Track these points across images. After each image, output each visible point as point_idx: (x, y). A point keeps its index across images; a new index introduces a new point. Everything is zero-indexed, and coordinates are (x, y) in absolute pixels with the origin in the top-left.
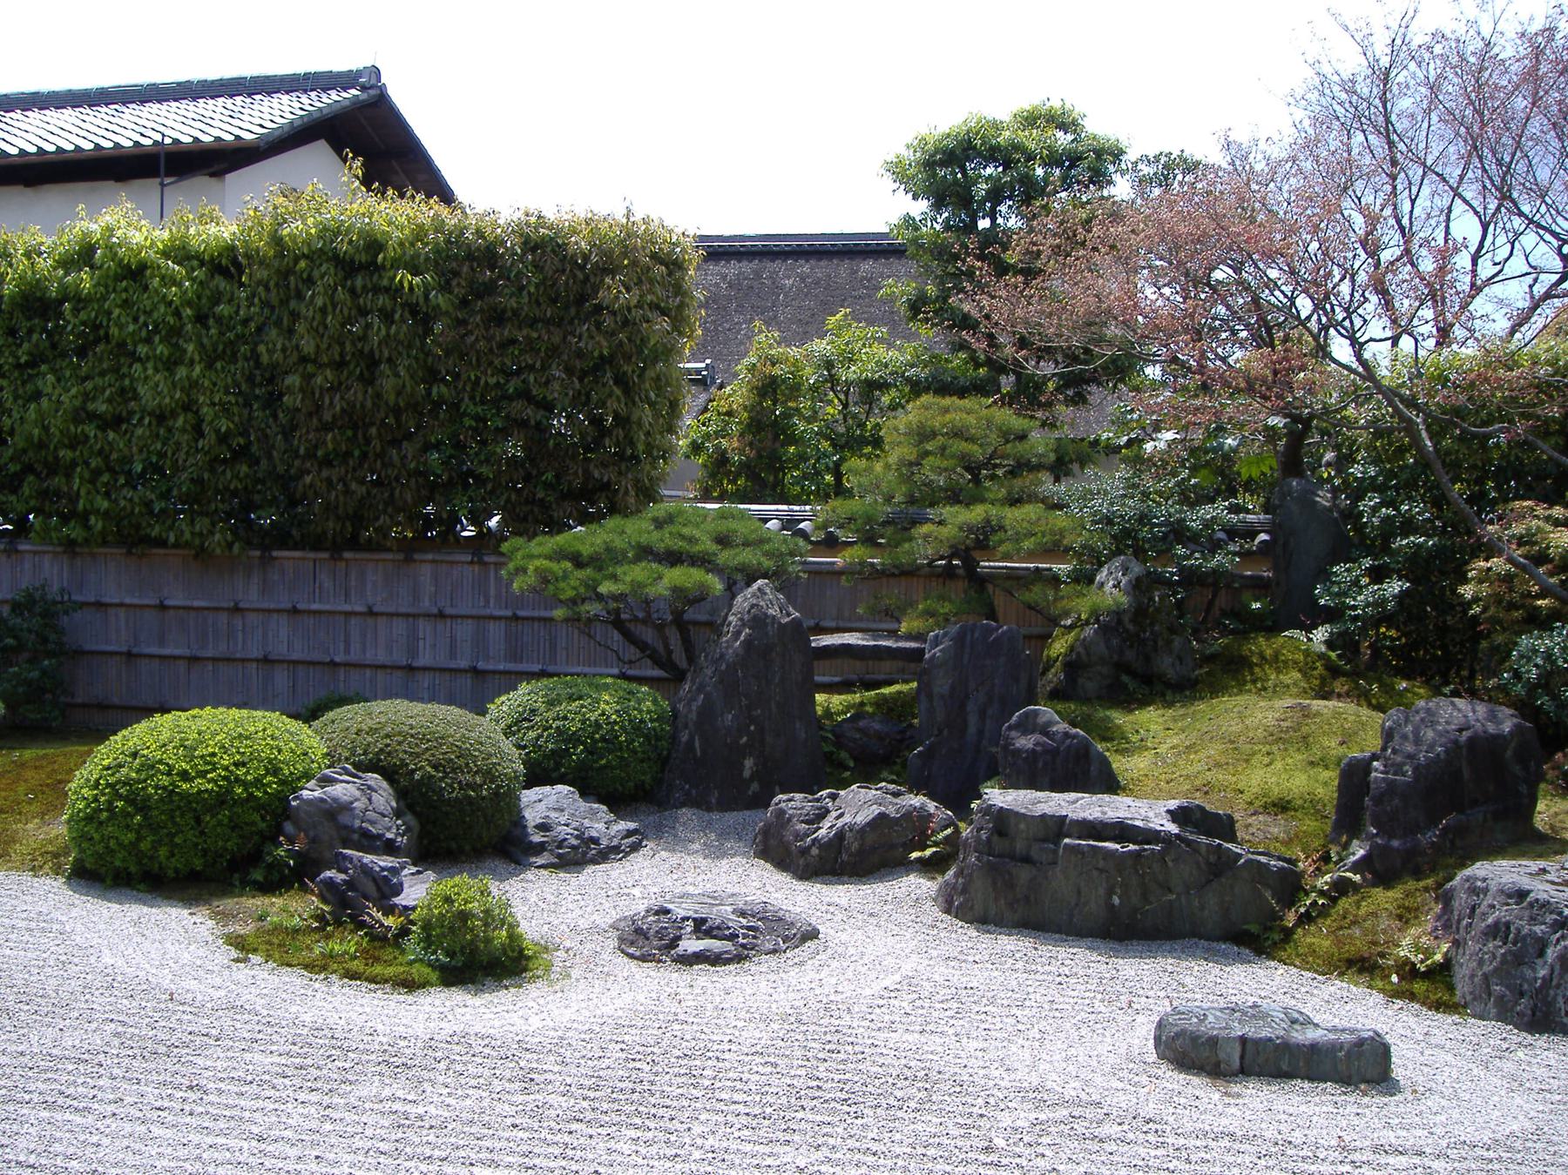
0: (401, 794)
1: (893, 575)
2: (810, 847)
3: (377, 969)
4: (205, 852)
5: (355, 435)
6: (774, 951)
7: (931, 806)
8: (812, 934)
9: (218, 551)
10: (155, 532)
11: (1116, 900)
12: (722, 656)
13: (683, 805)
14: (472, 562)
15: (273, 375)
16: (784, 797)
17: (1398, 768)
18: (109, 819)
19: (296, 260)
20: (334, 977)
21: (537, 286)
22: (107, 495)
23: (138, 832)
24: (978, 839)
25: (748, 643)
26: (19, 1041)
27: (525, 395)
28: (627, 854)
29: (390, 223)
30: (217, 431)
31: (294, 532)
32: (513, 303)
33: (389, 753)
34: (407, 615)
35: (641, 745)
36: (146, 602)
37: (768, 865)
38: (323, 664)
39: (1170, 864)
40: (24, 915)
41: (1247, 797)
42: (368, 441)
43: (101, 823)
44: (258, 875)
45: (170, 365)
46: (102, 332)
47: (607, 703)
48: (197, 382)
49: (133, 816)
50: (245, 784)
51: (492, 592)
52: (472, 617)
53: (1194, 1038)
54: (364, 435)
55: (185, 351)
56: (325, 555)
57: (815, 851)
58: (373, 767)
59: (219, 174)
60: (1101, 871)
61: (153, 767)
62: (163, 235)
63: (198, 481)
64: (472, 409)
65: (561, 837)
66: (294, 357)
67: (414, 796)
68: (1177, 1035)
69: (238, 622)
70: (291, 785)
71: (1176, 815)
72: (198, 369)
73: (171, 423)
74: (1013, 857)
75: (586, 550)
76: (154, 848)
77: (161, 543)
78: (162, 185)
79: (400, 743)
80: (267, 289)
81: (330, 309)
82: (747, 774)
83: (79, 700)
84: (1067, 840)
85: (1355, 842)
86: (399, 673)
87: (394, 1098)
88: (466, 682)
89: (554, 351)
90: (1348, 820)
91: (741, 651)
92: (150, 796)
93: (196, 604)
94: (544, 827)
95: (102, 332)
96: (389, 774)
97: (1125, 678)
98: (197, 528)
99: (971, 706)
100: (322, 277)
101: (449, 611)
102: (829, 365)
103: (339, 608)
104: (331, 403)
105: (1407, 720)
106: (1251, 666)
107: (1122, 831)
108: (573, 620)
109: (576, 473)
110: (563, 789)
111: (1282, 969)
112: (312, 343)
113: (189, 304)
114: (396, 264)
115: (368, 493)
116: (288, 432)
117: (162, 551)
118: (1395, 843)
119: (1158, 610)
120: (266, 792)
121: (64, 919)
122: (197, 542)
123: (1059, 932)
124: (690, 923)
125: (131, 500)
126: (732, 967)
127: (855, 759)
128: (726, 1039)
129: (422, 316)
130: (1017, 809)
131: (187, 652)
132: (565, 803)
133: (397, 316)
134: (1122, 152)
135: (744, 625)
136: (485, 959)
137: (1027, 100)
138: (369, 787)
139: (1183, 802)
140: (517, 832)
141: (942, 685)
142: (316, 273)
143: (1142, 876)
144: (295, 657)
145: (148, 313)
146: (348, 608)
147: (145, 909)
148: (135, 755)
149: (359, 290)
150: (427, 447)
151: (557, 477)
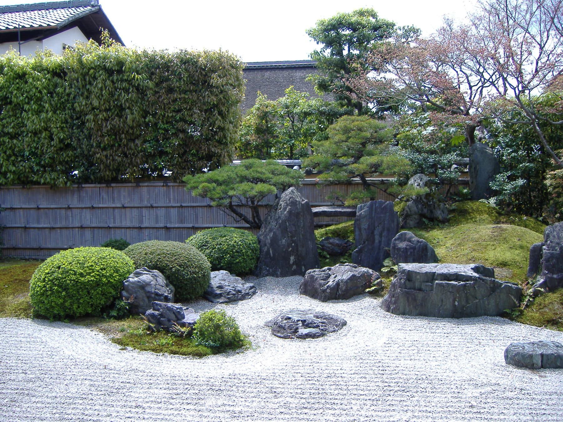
0: (167, 278)
1: (336, 184)
2: (326, 289)
3: (184, 349)
4: (92, 305)
5: (116, 138)
6: (334, 331)
7: (370, 271)
8: (345, 324)
9: (62, 185)
10: (35, 178)
11: (456, 303)
12: (279, 217)
13: (267, 275)
14: (163, 186)
15: (81, 115)
16: (312, 270)
17: (553, 248)
18: (51, 294)
19: (89, 70)
20: (166, 354)
21: (187, 77)
22: (14, 165)
23: (64, 299)
24: (400, 283)
25: (290, 212)
26: (51, 391)
27: (183, 120)
28: (252, 296)
29: (126, 55)
30: (59, 138)
31: (92, 177)
32: (178, 84)
33: (161, 261)
34: (138, 207)
35: (251, 253)
36: (32, 206)
37: (307, 297)
38: (105, 228)
39: (477, 288)
40: (23, 336)
41: (490, 261)
42: (121, 140)
43: (47, 296)
44: (114, 313)
45: (38, 113)
46: (9, 100)
47: (237, 237)
48: (50, 119)
49: (61, 293)
50: (106, 277)
51: (172, 197)
52: (164, 207)
53: (523, 356)
54: (119, 138)
55: (44, 107)
56: (104, 185)
57: (328, 291)
58: (155, 267)
59: (40, 40)
60: (451, 292)
61: (68, 272)
62: (32, 61)
63: (52, 158)
64: (162, 126)
65: (228, 291)
66: (90, 108)
67: (172, 278)
68: (516, 355)
69: (69, 213)
70: (124, 276)
71: (476, 269)
72: (50, 114)
73: (39, 136)
74: (414, 289)
75: (220, 179)
76: (71, 305)
77: (38, 183)
78: (20, 44)
79: (164, 257)
80: (78, 81)
81: (104, 88)
82: (291, 262)
83: (6, 247)
84: (436, 282)
85: (539, 277)
86: (136, 230)
87: (224, 405)
88: (163, 231)
89: (194, 103)
90: (535, 268)
91: (287, 215)
92: (68, 284)
93: (52, 206)
94: (220, 287)
95: (9, 100)
96: (162, 270)
97: (424, 220)
98: (53, 177)
99: (376, 232)
100: (100, 76)
101: (155, 205)
102: (287, 107)
103: (111, 206)
104: (106, 125)
105: (554, 230)
106: (469, 213)
107: (457, 277)
108: (219, 206)
109: (205, 150)
110: (225, 272)
111: (523, 326)
112: (98, 102)
113: (45, 88)
114: (131, 70)
115: (122, 160)
116: (89, 137)
117: (37, 186)
118: (555, 276)
119: (434, 194)
120: (115, 280)
121: (40, 336)
122: (52, 182)
123: (434, 316)
124: (300, 322)
125: (24, 166)
126: (321, 339)
127: (329, 255)
128: (339, 368)
129: (140, 90)
130: (416, 271)
131: (49, 226)
132: (225, 277)
133: (131, 91)
134: (394, 25)
135: (287, 205)
136: (228, 342)
137: (358, 8)
138: (156, 276)
139: (477, 265)
140: (210, 290)
141: (365, 225)
142: (97, 75)
143: (466, 294)
144: (93, 225)
145: (28, 92)
146: (114, 205)
147: (72, 330)
148: (59, 268)
149: (115, 81)
150: (145, 141)
151: (197, 151)
